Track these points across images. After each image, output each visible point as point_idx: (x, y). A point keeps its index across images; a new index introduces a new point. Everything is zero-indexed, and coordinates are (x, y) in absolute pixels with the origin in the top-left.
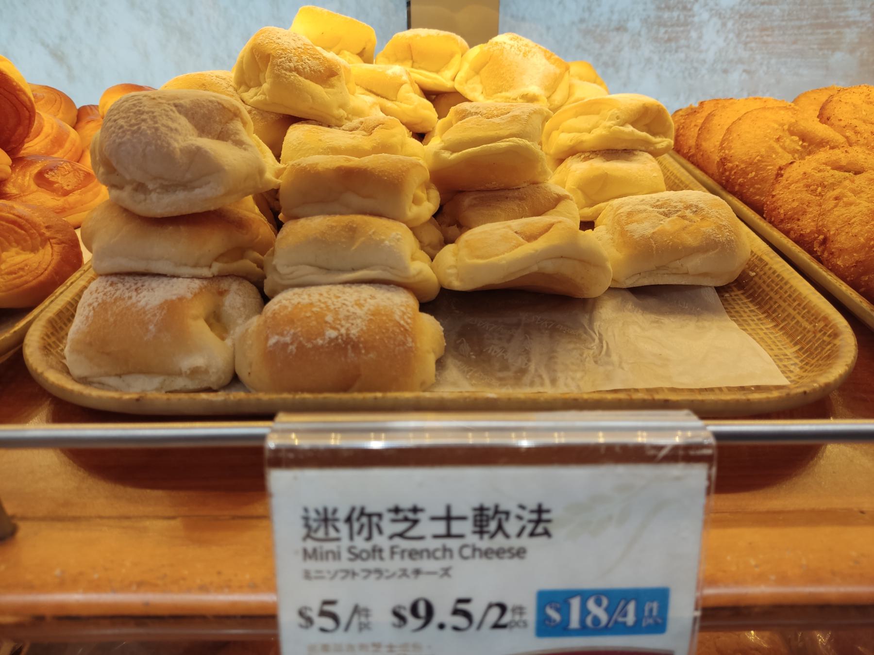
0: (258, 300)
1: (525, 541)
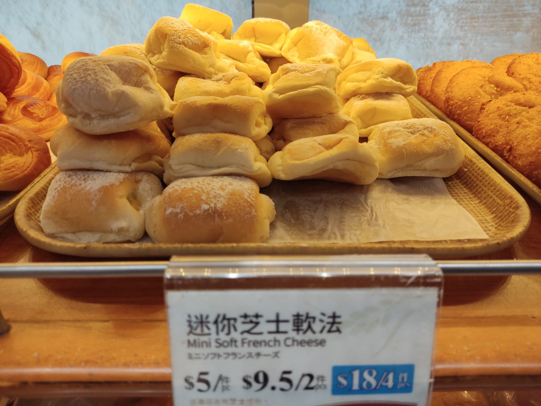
0: (160, 186)
1: (325, 335)
